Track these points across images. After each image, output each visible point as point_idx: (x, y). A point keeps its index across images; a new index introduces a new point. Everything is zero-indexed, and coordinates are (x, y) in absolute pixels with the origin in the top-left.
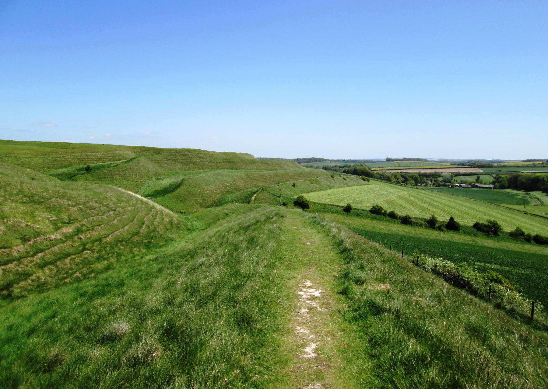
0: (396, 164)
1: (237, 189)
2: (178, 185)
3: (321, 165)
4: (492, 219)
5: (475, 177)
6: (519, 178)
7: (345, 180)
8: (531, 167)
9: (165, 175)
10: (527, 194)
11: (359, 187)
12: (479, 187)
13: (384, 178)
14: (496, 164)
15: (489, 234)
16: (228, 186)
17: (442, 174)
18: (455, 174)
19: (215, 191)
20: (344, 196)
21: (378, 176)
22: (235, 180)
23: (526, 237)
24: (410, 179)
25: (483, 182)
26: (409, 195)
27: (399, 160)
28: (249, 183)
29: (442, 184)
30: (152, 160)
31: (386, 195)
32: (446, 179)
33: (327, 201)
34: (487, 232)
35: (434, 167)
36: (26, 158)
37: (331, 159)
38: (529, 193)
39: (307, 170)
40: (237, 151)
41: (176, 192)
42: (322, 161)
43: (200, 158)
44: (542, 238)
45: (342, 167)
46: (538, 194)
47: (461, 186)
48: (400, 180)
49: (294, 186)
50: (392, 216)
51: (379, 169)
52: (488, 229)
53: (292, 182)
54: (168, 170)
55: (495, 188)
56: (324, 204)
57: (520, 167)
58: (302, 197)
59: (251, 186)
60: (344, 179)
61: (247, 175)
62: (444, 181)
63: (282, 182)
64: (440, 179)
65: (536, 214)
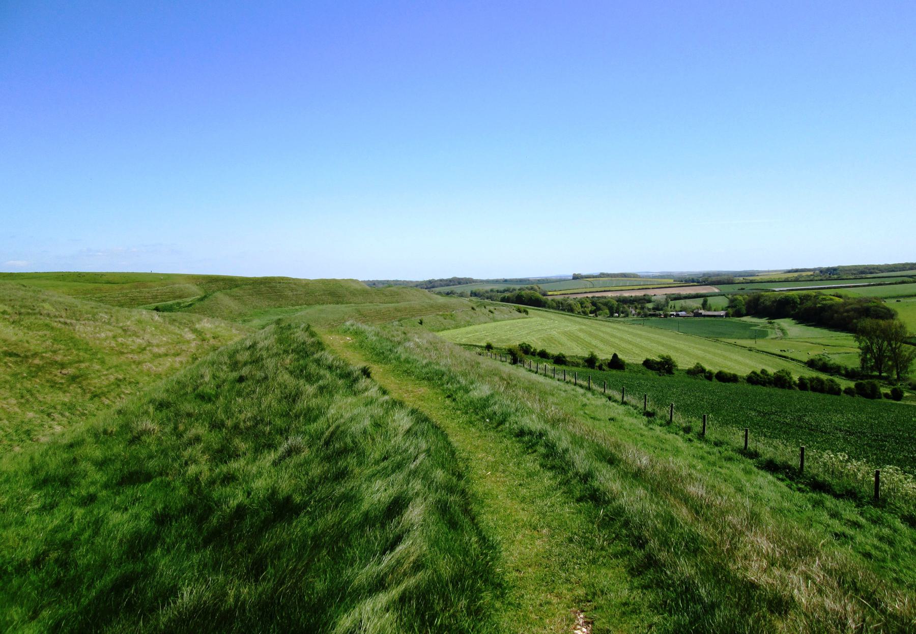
0: (589, 284)
3: (468, 289)
4: (665, 355)
5: (701, 300)
6: (761, 300)
7: (492, 312)
8: (791, 281)
9: (251, 316)
10: (770, 323)
11: (512, 321)
12: (705, 316)
13: (564, 307)
14: (741, 279)
15: (660, 372)
17: (653, 298)
18: (674, 296)
20: (487, 334)
21: (555, 304)
23: (706, 374)
24: (602, 307)
25: (713, 308)
26: (581, 330)
27: (594, 277)
29: (651, 313)
30: (231, 296)
31: (546, 330)
32: (658, 305)
34: (659, 369)
35: (641, 287)
37: (485, 278)
38: (773, 321)
39: (441, 300)
40: (338, 277)
42: (470, 283)
43: (292, 290)
44: (726, 374)
45: (501, 292)
46: (786, 323)
47: (678, 315)
48: (588, 310)
49: (421, 323)
50: (543, 355)
51: (559, 293)
52: (659, 366)
53: (418, 319)
55: (727, 315)
57: (775, 282)
60: (490, 311)
61: (359, 311)
62: (656, 308)
63: (404, 319)
64: (650, 306)
65: (766, 350)
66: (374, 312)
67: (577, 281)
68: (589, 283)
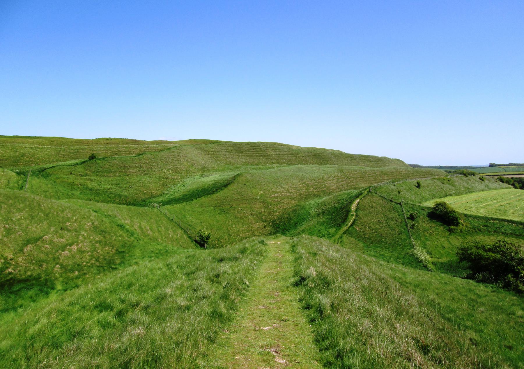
1: (326, 192)
2: (226, 185)
16: (312, 186)
19: (288, 194)
22: (323, 177)
27: (504, 165)
28: (344, 182)
33: (482, 212)
36: (32, 148)
41: (220, 194)
53: (415, 181)
54: (226, 164)
56: (484, 218)
58: (443, 205)
59: (348, 188)
66: (359, 173)
67: (493, 168)
68: (502, 169)
